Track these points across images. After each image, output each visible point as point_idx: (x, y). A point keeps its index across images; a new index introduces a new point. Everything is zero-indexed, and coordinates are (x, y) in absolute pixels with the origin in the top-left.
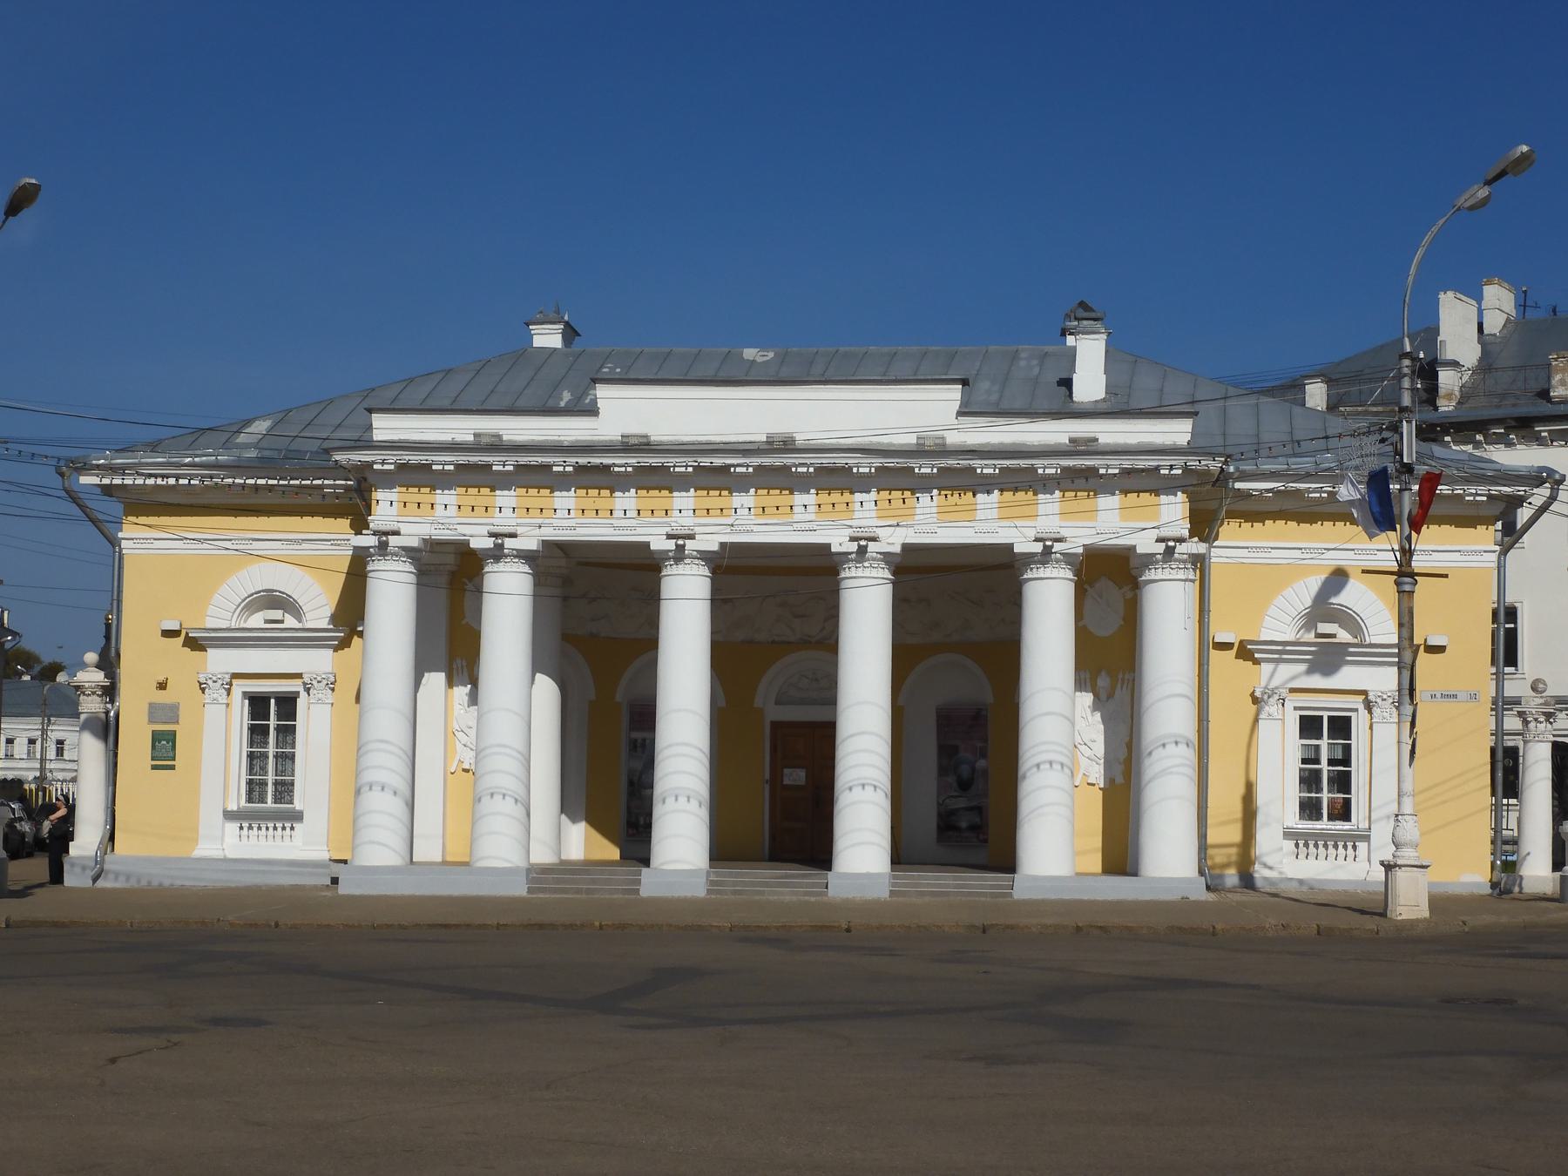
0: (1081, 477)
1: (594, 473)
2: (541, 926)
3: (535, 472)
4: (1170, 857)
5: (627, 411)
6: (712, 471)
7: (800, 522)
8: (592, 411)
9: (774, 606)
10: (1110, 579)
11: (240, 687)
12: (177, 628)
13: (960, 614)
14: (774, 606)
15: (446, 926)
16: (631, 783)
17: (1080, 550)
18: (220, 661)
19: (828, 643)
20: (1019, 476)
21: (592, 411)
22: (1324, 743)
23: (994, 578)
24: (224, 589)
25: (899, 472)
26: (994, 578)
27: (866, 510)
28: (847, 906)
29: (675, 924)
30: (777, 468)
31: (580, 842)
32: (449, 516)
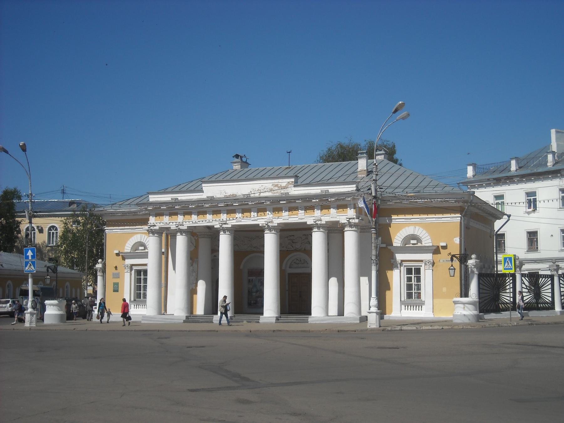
0: (324, 202)
1: (201, 208)
2: (556, 323)
3: (186, 209)
4: (350, 309)
5: (213, 191)
6: (230, 206)
7: (253, 219)
8: (202, 191)
9: (248, 243)
10: (334, 232)
11: (134, 268)
12: (445, 245)
13: (295, 242)
14: (248, 243)
15: (114, 331)
16: (249, 291)
17: (276, 225)
18: (129, 262)
19: (309, 253)
20: (308, 203)
21: (202, 191)
22: (413, 276)
23: (305, 231)
24: (129, 242)
25: (276, 204)
26: (305, 231)
27: (269, 216)
28: (265, 324)
29: (50, 331)
30: (245, 205)
31: (534, 301)
32: (166, 221)
